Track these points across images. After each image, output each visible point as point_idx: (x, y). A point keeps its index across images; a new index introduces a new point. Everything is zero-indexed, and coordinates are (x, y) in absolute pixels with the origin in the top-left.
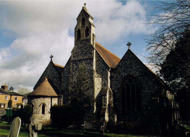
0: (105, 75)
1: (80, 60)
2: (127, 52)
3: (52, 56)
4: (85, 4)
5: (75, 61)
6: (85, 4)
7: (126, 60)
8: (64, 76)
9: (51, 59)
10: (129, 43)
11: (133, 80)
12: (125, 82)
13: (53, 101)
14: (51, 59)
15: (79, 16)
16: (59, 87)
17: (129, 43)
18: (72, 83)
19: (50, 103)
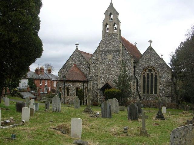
0: (130, 65)
1: (108, 51)
2: (149, 48)
3: (77, 43)
4: (150, 42)
5: (104, 51)
6: (150, 42)
7: (148, 54)
8: (92, 63)
9: (77, 47)
10: (150, 40)
11: (153, 70)
12: (146, 71)
13: (65, 85)
14: (77, 47)
15: (107, 11)
16: (86, 72)
17: (150, 40)
18: (101, 70)
19: (83, 87)
